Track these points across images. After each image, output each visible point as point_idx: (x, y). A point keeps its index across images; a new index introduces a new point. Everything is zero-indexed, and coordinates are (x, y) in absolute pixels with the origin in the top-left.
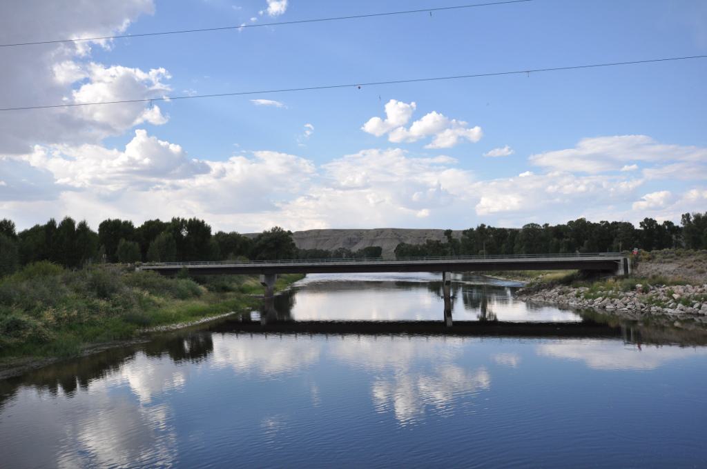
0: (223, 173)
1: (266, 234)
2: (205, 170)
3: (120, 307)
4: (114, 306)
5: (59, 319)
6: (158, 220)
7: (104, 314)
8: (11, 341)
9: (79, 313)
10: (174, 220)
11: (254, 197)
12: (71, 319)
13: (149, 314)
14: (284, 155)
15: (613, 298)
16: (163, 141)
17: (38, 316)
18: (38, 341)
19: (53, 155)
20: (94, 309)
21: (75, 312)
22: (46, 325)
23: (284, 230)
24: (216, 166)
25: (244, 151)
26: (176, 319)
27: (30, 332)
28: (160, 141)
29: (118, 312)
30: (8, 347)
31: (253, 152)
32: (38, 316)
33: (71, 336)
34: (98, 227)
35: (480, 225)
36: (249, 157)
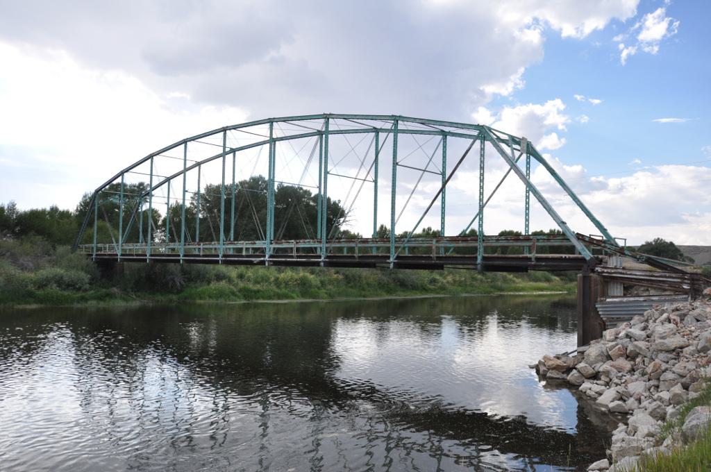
0: (621, 189)
1: (643, 246)
2: (603, 187)
3: (489, 280)
4: (487, 279)
5: (455, 281)
6: (542, 231)
7: (479, 282)
8: (432, 287)
9: (465, 280)
10: (551, 231)
11: (656, 209)
12: (461, 282)
13: (504, 286)
14: (692, 168)
15: (592, 364)
16: (571, 165)
17: (445, 278)
18: (443, 288)
19: (267, 178)
20: (474, 279)
21: (463, 279)
22: (448, 282)
23: (666, 241)
24: (613, 182)
25: (647, 167)
26: (522, 289)
27: (440, 284)
28: (565, 167)
29: (487, 282)
30: (430, 289)
31: (657, 167)
32: (445, 278)
33: (460, 289)
34: (534, 231)
35: (426, 228)
36: (654, 172)
